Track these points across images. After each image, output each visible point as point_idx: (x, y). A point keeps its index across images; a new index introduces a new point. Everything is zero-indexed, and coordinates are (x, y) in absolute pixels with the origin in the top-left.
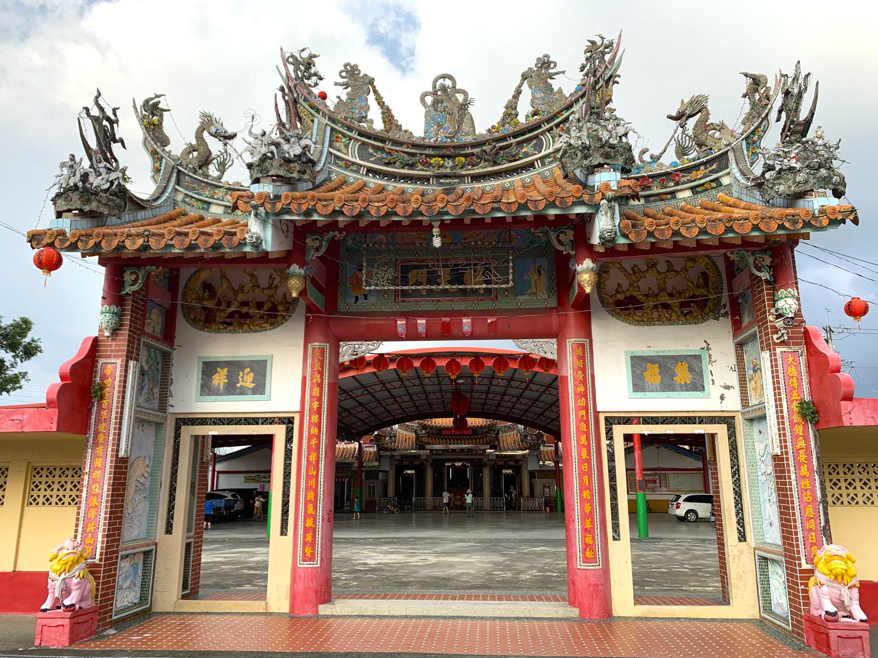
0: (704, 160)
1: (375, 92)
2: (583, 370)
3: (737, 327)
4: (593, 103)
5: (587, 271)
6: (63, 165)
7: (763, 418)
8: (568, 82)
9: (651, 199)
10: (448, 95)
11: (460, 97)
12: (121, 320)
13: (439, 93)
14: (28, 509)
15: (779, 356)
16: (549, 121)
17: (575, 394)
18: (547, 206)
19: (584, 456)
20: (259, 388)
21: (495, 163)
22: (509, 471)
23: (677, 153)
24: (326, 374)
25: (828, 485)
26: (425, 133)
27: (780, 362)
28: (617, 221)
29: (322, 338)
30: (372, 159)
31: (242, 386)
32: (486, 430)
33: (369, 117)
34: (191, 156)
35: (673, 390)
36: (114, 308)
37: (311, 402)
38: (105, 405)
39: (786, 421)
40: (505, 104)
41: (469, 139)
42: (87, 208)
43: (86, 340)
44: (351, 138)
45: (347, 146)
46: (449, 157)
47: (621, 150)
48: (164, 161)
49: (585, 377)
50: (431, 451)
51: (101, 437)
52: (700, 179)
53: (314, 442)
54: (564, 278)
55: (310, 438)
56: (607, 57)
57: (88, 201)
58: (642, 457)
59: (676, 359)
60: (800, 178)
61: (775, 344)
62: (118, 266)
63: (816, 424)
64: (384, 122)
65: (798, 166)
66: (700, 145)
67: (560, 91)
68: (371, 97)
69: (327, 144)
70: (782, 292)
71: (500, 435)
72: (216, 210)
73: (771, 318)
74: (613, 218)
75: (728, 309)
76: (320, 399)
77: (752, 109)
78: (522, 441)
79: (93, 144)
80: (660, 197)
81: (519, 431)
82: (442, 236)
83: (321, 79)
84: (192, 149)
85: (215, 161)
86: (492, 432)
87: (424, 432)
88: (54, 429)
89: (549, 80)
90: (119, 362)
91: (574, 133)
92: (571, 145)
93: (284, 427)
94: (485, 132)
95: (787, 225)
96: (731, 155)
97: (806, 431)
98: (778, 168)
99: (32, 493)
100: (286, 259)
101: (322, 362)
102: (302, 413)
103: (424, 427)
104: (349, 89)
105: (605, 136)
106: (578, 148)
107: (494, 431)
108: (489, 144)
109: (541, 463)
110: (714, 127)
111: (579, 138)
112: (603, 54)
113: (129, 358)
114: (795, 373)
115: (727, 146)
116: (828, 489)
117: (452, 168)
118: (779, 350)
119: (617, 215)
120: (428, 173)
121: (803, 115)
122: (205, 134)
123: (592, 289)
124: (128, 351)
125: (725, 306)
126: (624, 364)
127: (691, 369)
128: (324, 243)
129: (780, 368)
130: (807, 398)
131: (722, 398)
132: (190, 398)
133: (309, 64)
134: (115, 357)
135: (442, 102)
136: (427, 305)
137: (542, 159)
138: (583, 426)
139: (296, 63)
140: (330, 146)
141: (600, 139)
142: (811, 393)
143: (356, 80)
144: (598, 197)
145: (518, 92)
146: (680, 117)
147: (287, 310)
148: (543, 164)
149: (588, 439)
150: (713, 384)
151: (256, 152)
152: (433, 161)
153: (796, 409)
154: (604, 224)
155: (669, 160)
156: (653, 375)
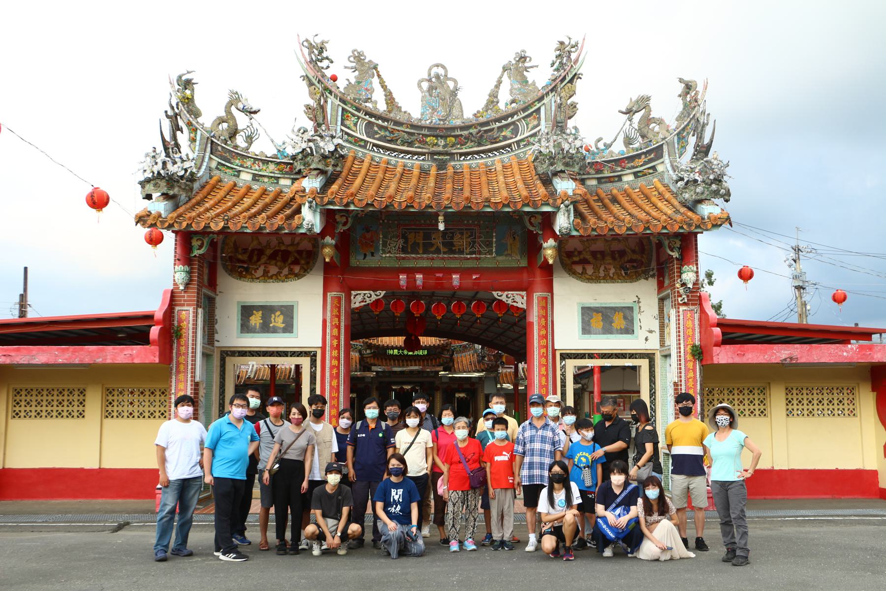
0: (645, 150)
1: (379, 76)
2: (546, 317)
3: (661, 286)
4: (558, 119)
5: (550, 248)
6: (147, 155)
7: (669, 355)
8: (541, 75)
9: (603, 180)
10: (441, 83)
11: (451, 84)
12: (191, 277)
13: (434, 80)
14: (106, 421)
15: (681, 313)
16: (524, 110)
17: (539, 336)
18: (523, 206)
19: (544, 383)
20: (288, 328)
21: (480, 145)
22: (462, 395)
23: (625, 143)
24: (343, 318)
25: (706, 403)
26: (422, 114)
27: (681, 317)
28: (572, 218)
29: (338, 289)
30: (377, 136)
31: (274, 326)
32: (439, 350)
33: (373, 99)
34: (220, 127)
35: (611, 333)
36: (187, 268)
37: (331, 340)
38: (183, 343)
39: (682, 358)
40: (488, 92)
41: (458, 122)
42: (171, 193)
43: (165, 292)
44: (359, 118)
45: (355, 125)
46: (442, 137)
47: (577, 160)
48: (199, 132)
49: (546, 323)
50: (377, 372)
51: (182, 367)
52: (641, 166)
53: (335, 371)
54: (533, 248)
55: (332, 368)
56: (573, 56)
57: (171, 187)
58: (600, 380)
59: (615, 309)
60: (699, 189)
61: (679, 304)
62: (186, 238)
63: (701, 361)
64: (387, 103)
65: (699, 179)
66: (643, 137)
67: (534, 83)
68: (375, 81)
69: (339, 123)
70: (685, 268)
71: (455, 355)
72: (246, 177)
73: (678, 285)
74: (569, 218)
75: (655, 271)
76: (338, 338)
77: (684, 109)
78: (479, 362)
79: (168, 138)
80: (610, 180)
81: (476, 351)
82: (445, 221)
83: (332, 62)
84: (221, 120)
85: (242, 133)
86: (446, 352)
87: (368, 351)
88: (157, 360)
89: (525, 73)
90: (191, 309)
91: (544, 143)
92: (541, 152)
93: (309, 359)
94: (471, 117)
95: (685, 227)
96: (665, 148)
97: (694, 366)
98: (686, 180)
99: (107, 409)
100: (323, 234)
101: (339, 308)
102: (323, 348)
103: (370, 346)
104: (357, 73)
105: (566, 147)
106: (546, 155)
107: (448, 351)
108: (476, 128)
109: (499, 386)
110: (654, 120)
111: (547, 147)
112: (569, 52)
113: (198, 306)
114: (691, 326)
115: (663, 139)
116: (706, 406)
117: (445, 146)
118: (682, 308)
119: (572, 215)
120: (424, 150)
121: (706, 141)
122: (233, 109)
123: (554, 261)
124: (198, 301)
125: (653, 270)
126: (576, 313)
127: (625, 318)
128: (350, 219)
129: (681, 322)
130: (697, 343)
131: (646, 339)
132: (231, 335)
133: (321, 50)
134: (188, 305)
135: (436, 89)
136: (425, 264)
137: (518, 142)
138: (544, 360)
139: (311, 47)
140: (342, 124)
141: (563, 150)
142: (701, 340)
143: (363, 65)
144: (559, 201)
145: (499, 82)
146: (629, 112)
147: (308, 263)
148: (519, 146)
149: (547, 370)
150: (711, 283)
151: (297, 146)
152: (428, 139)
153: (689, 351)
154: (563, 222)
155: (619, 149)
156: (597, 322)
